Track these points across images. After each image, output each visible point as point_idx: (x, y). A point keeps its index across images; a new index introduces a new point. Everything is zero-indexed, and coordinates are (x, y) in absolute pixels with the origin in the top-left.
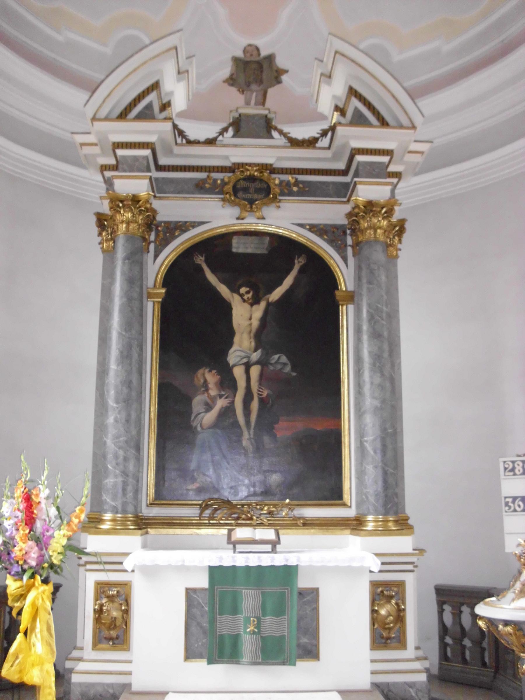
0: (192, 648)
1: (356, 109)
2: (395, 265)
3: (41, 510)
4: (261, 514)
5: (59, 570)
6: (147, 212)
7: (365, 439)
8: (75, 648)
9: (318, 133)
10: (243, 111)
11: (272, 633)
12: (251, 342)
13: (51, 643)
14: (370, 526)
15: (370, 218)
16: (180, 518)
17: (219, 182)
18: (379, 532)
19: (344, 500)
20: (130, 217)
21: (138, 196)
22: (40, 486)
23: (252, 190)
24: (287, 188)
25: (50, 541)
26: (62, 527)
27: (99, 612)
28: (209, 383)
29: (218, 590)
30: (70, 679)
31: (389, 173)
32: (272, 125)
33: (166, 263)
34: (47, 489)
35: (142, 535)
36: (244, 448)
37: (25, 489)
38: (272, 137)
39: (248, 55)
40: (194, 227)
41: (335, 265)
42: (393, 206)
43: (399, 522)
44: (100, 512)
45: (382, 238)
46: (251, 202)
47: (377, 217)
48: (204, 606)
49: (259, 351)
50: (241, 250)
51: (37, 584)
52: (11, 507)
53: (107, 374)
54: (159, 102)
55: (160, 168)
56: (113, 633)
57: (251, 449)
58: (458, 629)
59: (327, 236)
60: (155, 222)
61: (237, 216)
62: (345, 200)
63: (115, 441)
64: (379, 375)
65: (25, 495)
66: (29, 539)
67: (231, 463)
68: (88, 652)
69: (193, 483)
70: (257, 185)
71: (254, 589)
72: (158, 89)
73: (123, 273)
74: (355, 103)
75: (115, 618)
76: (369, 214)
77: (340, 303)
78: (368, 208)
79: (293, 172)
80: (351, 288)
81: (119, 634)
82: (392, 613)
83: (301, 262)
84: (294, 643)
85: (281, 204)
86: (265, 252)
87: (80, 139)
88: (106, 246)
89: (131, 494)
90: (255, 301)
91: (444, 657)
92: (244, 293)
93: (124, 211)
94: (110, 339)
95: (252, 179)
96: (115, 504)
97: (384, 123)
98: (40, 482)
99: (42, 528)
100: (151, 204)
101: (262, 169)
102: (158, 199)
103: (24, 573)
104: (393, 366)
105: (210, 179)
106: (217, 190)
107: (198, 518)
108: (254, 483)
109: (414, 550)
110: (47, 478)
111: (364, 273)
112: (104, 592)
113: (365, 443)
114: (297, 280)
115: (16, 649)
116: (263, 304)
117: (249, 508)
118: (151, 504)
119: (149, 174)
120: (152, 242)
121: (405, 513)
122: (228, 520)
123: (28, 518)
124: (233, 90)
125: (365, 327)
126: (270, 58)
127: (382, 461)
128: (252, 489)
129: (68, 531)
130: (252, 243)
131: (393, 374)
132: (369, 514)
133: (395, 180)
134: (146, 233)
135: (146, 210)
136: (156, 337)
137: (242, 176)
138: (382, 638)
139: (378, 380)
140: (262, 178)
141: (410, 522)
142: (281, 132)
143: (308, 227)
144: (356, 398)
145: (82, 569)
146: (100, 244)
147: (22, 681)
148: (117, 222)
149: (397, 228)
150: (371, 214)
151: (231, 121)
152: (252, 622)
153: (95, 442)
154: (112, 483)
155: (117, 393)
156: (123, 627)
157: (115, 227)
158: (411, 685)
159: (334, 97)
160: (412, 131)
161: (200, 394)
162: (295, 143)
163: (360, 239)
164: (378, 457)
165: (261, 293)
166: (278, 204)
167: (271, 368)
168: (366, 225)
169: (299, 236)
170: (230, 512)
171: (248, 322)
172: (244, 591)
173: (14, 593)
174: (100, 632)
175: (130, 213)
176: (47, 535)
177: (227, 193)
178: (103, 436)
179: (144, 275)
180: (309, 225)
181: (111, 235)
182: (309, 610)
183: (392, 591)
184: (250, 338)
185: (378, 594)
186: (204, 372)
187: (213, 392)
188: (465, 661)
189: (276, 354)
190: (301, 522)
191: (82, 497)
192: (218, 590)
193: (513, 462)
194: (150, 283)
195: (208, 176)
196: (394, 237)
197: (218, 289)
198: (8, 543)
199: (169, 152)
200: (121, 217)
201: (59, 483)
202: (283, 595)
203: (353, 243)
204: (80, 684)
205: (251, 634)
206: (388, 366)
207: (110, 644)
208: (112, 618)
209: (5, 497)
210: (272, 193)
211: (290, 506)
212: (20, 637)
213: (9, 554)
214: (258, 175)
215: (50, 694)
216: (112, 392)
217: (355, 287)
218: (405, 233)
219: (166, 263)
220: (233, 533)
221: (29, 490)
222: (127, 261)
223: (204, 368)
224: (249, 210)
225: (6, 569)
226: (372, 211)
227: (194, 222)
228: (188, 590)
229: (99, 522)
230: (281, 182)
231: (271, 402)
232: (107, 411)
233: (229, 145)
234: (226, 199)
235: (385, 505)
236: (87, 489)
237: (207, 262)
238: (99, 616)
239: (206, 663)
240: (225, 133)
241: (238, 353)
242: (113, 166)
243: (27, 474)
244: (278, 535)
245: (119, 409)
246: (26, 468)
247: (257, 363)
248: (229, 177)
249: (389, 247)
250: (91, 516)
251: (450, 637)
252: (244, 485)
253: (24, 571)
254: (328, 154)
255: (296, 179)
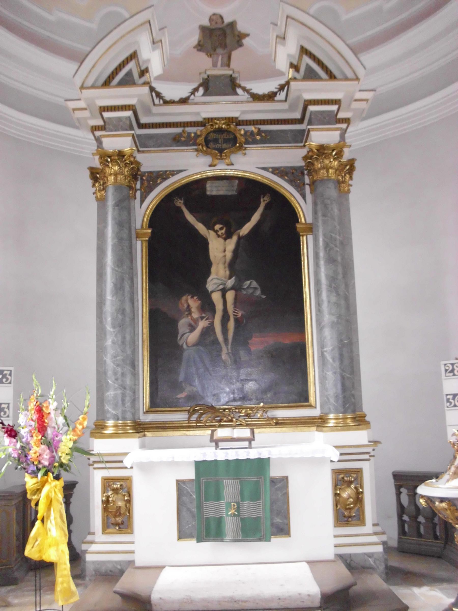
0: (184, 529)
1: (307, 65)
2: (347, 200)
3: (51, 419)
4: (239, 417)
5: (68, 468)
6: (132, 165)
7: (325, 349)
8: (89, 533)
9: (276, 88)
10: (209, 73)
11: (249, 515)
12: (226, 271)
13: (64, 527)
14: (332, 423)
15: (323, 160)
16: (172, 422)
17: (193, 135)
18: (339, 428)
19: (310, 402)
20: (117, 170)
21: (124, 151)
22: (50, 400)
23: (221, 141)
24: (251, 137)
25: (59, 445)
26: (69, 432)
27: (106, 502)
28: (192, 308)
29: (203, 480)
30: (85, 558)
31: (339, 119)
32: (237, 83)
33: (151, 207)
34: (56, 402)
35: (139, 437)
36: (223, 361)
37: (37, 402)
38: (236, 94)
39: (214, 23)
40: (173, 175)
41: (295, 202)
42: (342, 148)
43: (357, 419)
44: (104, 420)
45: (333, 177)
46: (221, 151)
47: (328, 158)
48: (192, 494)
49: (233, 278)
50: (214, 193)
51: (49, 480)
52: (26, 418)
53: (105, 304)
54: (138, 69)
55: (141, 126)
56: (119, 520)
57: (229, 362)
58: (413, 508)
59: (287, 177)
60: (139, 173)
61: (209, 163)
62: (302, 144)
63: (113, 360)
64: (335, 294)
65: (37, 407)
66: (41, 444)
67: (213, 374)
68: (99, 536)
69: (182, 392)
70: (225, 135)
71: (233, 479)
72: (136, 58)
73: (114, 218)
74: (307, 60)
75: (120, 507)
76: (322, 156)
77: (301, 234)
78: (322, 151)
79: (255, 123)
80: (310, 220)
81: (124, 520)
82: (352, 496)
83: (266, 200)
84: (268, 523)
85: (246, 151)
86: (235, 193)
87: (72, 105)
88: (99, 195)
89: (129, 404)
90: (228, 236)
91: (402, 532)
92: (218, 229)
93: (112, 165)
94: (106, 274)
95: (220, 131)
96: (116, 412)
97: (332, 76)
98: (50, 397)
99: (53, 434)
100: (135, 158)
101: (229, 122)
102: (141, 153)
103: (39, 472)
104: (347, 286)
105: (185, 133)
106: (191, 142)
107: (187, 422)
108: (234, 390)
109: (369, 442)
110: (55, 393)
111: (319, 207)
112: (109, 486)
113: (325, 353)
114: (263, 215)
115: (35, 534)
116: (235, 238)
117: (230, 411)
118: (147, 412)
119: (133, 132)
120: (138, 190)
121: (363, 412)
122: (212, 422)
123: (40, 427)
124: (202, 55)
125: (322, 254)
126: (232, 25)
127: (340, 368)
128: (232, 396)
129: (73, 435)
130: (223, 186)
131: (347, 293)
132: (330, 413)
133: (344, 126)
134: (132, 182)
135: (130, 163)
136: (146, 271)
137: (212, 129)
138: (345, 517)
139: (334, 299)
140: (229, 130)
141: (367, 418)
142: (244, 89)
143: (271, 170)
144: (317, 315)
145: (91, 467)
146: (94, 193)
147: (41, 559)
148: (107, 174)
149: (348, 167)
150: (323, 156)
151: (201, 81)
152: (232, 506)
153: (97, 362)
154: (112, 395)
155: (114, 319)
156: (127, 515)
157: (105, 179)
158: (370, 555)
159: (289, 56)
160: (357, 82)
161: (184, 317)
162: (256, 98)
163: (315, 178)
164: (337, 364)
165: (232, 230)
166: (244, 152)
167: (244, 292)
168: (319, 166)
169: (264, 178)
170: (213, 416)
171: (223, 254)
172: (225, 481)
173: (31, 488)
174: (108, 519)
175: (117, 167)
176: (56, 440)
177: (199, 145)
178: (104, 356)
179: (132, 219)
180: (272, 168)
181: (103, 186)
182: (281, 494)
183: (351, 477)
184: (225, 268)
185: (340, 480)
186: (187, 298)
187: (196, 315)
188: (419, 535)
189: (248, 280)
190: (275, 421)
191: (85, 407)
192: (203, 480)
193: (453, 364)
194: (138, 226)
195: (183, 131)
196: (345, 175)
197: (196, 227)
198: (25, 447)
199: (148, 112)
200: (109, 170)
201: (65, 396)
202: (257, 482)
203: (310, 182)
204: (94, 562)
205: (232, 516)
206: (343, 287)
207: (116, 529)
208: (117, 507)
209: (21, 410)
210: (238, 142)
211: (265, 410)
212: (38, 524)
213: (26, 456)
214: (226, 127)
215: (65, 569)
216: (109, 319)
217: (313, 220)
218: (354, 170)
219: (151, 207)
220: (215, 433)
221: (41, 404)
222: (116, 208)
223: (187, 295)
224: (219, 158)
225: (25, 469)
226: (324, 154)
227: (173, 171)
228: (178, 481)
229: (103, 428)
230: (246, 132)
231: (245, 321)
232: (105, 334)
233: (200, 103)
234: (199, 149)
235: (344, 406)
236: (88, 400)
237: (186, 205)
238: (106, 506)
239: (195, 542)
240: (196, 92)
241: (215, 281)
242: (102, 126)
243: (38, 390)
244: (253, 433)
245: (115, 333)
246: (37, 385)
247: (232, 288)
248: (201, 131)
249: (341, 184)
250: (97, 424)
251: (407, 515)
252: (226, 392)
253: (39, 470)
254: (285, 106)
255: (259, 129)
